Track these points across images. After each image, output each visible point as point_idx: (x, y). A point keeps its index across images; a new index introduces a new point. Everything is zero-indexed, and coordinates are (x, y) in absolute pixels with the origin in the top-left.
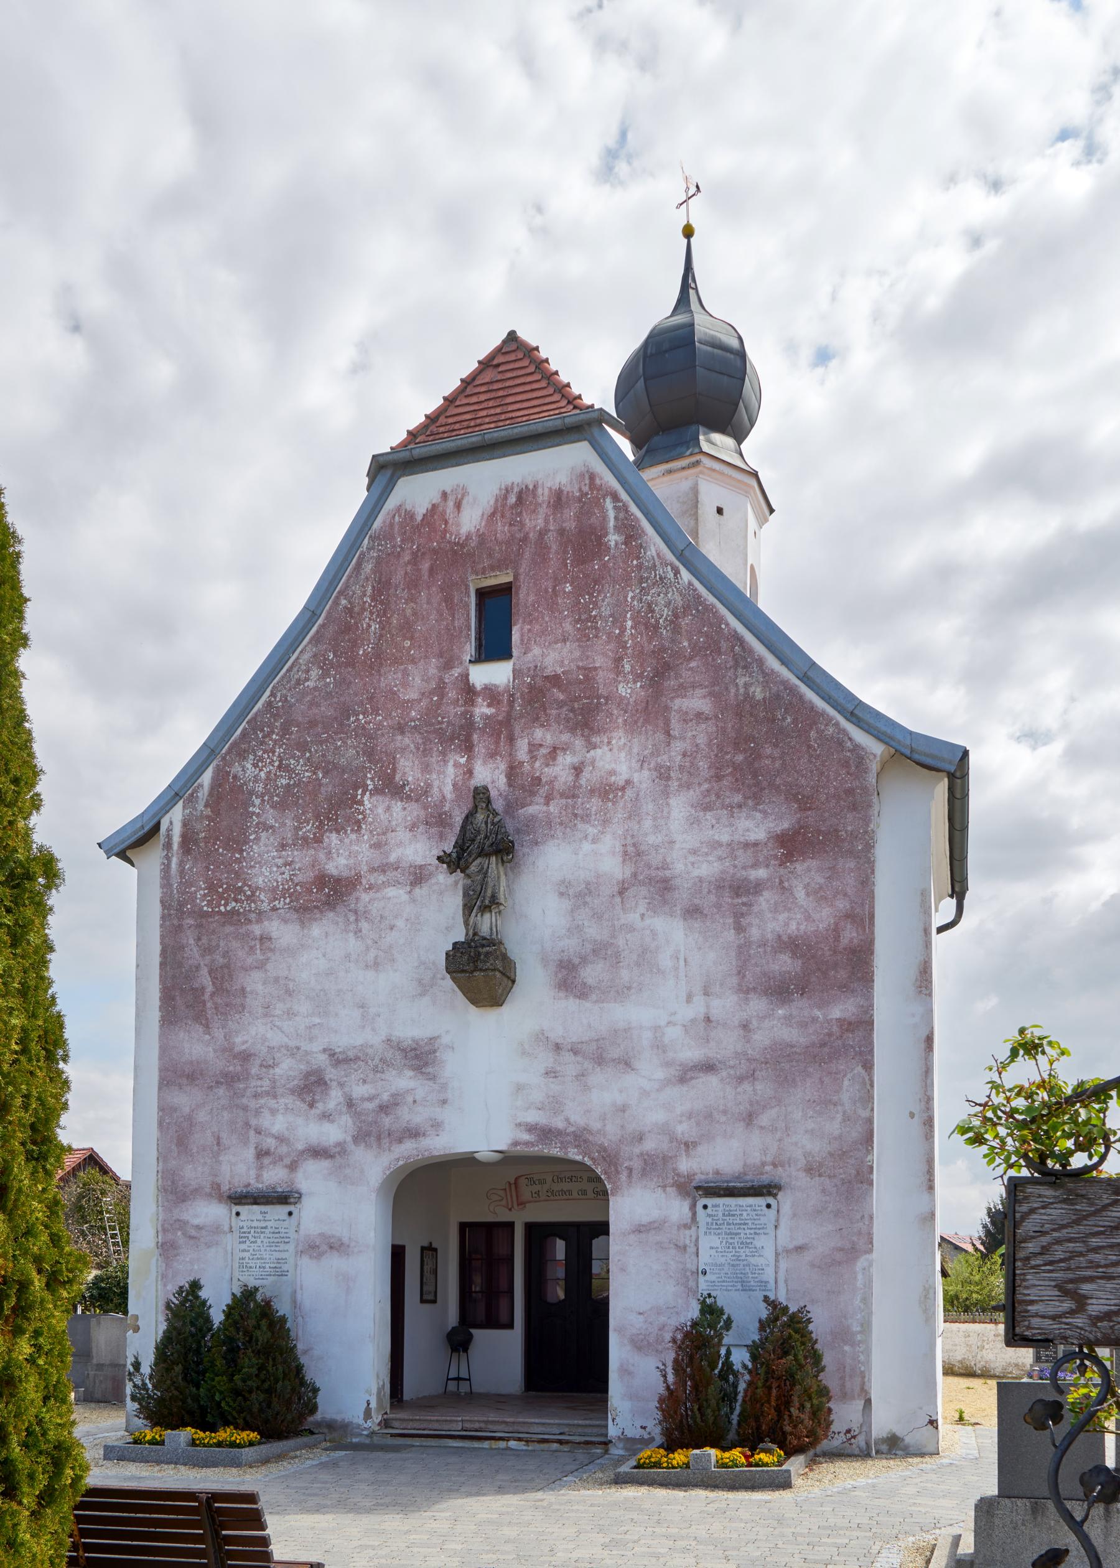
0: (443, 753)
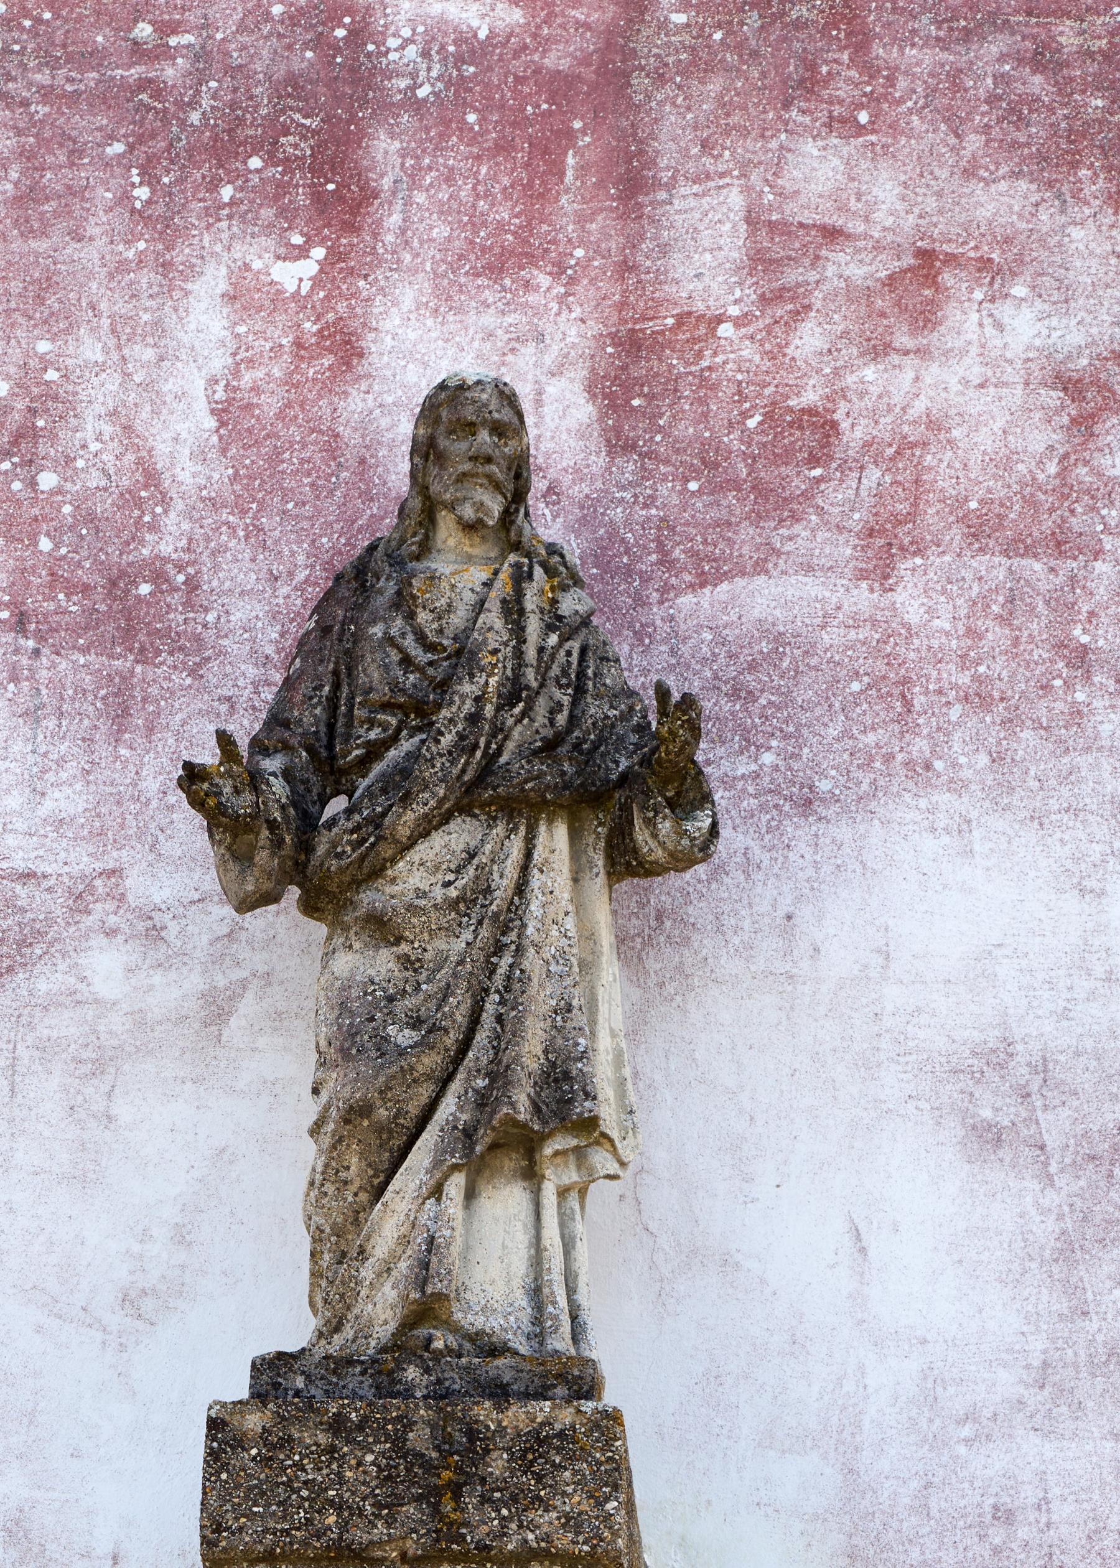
0: (162, 225)
